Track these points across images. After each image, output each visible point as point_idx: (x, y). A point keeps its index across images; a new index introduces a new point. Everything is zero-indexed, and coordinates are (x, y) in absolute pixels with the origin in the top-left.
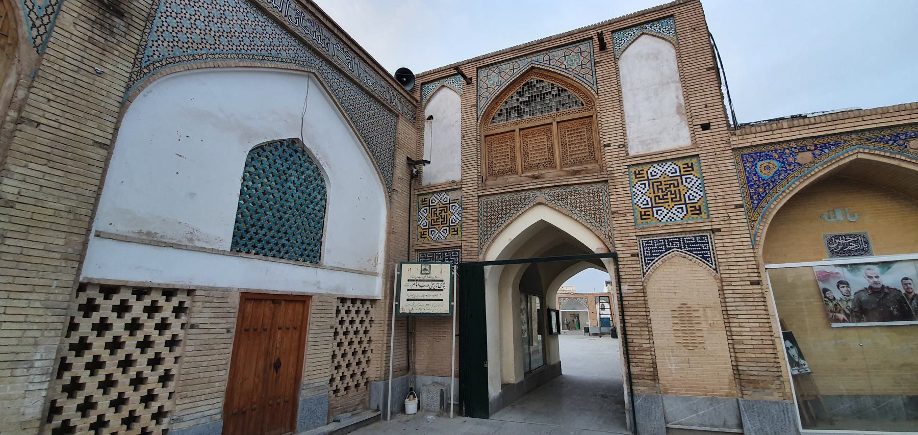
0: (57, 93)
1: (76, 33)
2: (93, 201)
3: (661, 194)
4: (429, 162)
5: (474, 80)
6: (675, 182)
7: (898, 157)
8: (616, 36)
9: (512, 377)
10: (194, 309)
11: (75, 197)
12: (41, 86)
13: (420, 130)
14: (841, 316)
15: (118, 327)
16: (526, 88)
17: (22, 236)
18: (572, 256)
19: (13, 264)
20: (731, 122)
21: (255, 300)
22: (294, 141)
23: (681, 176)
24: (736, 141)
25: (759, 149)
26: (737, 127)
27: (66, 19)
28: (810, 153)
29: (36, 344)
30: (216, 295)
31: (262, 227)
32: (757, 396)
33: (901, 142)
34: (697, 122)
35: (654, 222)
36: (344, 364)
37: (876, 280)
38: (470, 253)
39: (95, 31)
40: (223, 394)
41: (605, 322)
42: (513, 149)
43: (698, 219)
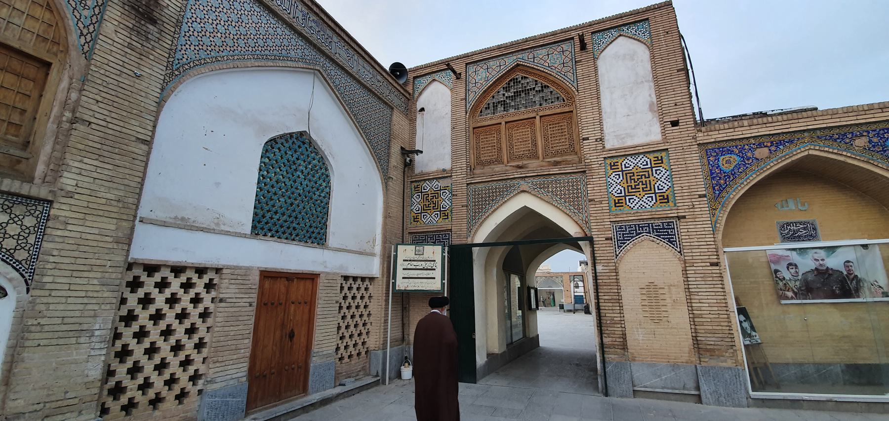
0: (104, 95)
1: (117, 39)
2: (138, 191)
3: (633, 184)
4: (422, 152)
5: (463, 75)
6: (646, 174)
7: (844, 153)
8: (595, 37)
9: (496, 347)
10: (222, 286)
11: (122, 187)
12: (90, 89)
13: (412, 121)
15: (160, 301)
16: (512, 84)
17: (81, 222)
18: (550, 238)
19: (74, 247)
20: (698, 118)
21: (271, 277)
22: (302, 134)
23: (652, 168)
24: (702, 137)
25: (722, 145)
26: (704, 123)
27: (108, 28)
28: (766, 150)
29: (95, 316)
30: (239, 273)
31: (276, 213)
32: (713, 363)
33: (848, 141)
34: (668, 119)
36: (347, 335)
37: (821, 262)
38: (459, 236)
39: (133, 37)
40: (247, 360)
41: (578, 299)
42: (499, 141)
43: (665, 207)
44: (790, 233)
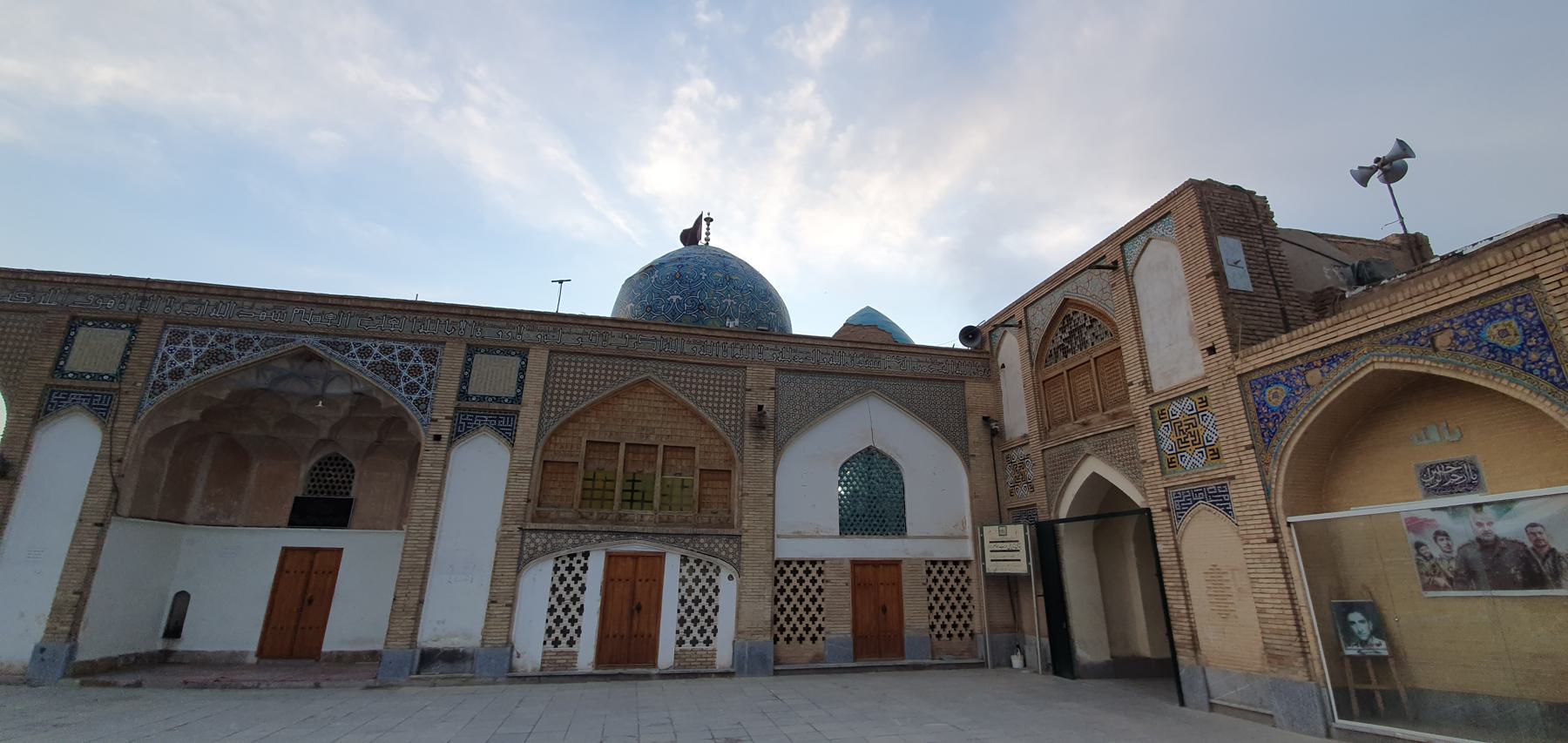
14: (1442, 581)
35: (1179, 469)
37: (1487, 528)
44: (1439, 480)
